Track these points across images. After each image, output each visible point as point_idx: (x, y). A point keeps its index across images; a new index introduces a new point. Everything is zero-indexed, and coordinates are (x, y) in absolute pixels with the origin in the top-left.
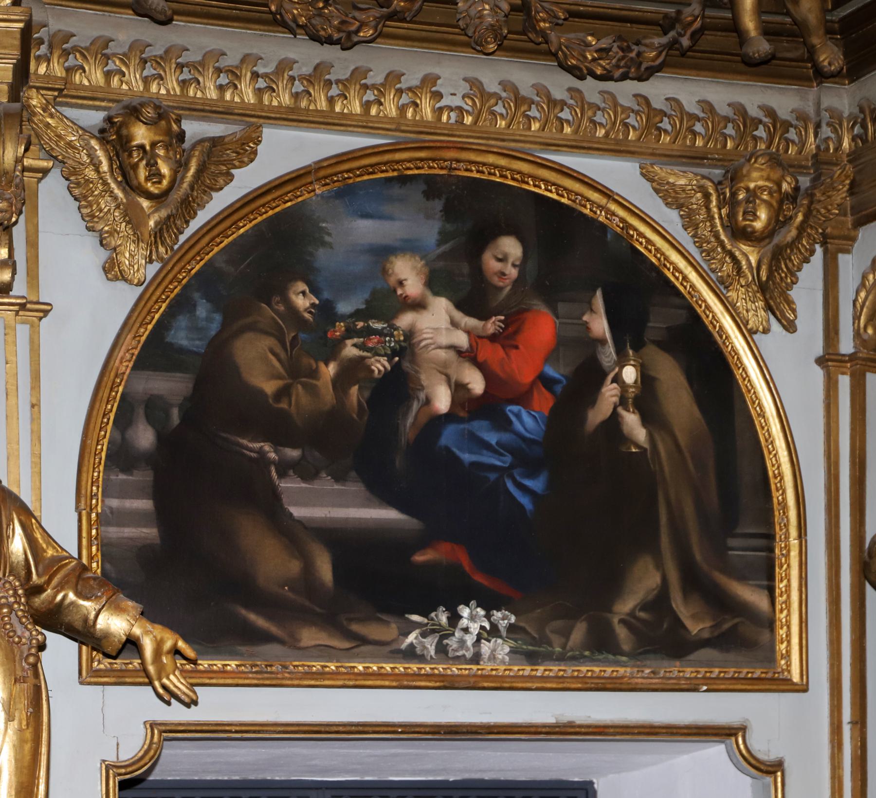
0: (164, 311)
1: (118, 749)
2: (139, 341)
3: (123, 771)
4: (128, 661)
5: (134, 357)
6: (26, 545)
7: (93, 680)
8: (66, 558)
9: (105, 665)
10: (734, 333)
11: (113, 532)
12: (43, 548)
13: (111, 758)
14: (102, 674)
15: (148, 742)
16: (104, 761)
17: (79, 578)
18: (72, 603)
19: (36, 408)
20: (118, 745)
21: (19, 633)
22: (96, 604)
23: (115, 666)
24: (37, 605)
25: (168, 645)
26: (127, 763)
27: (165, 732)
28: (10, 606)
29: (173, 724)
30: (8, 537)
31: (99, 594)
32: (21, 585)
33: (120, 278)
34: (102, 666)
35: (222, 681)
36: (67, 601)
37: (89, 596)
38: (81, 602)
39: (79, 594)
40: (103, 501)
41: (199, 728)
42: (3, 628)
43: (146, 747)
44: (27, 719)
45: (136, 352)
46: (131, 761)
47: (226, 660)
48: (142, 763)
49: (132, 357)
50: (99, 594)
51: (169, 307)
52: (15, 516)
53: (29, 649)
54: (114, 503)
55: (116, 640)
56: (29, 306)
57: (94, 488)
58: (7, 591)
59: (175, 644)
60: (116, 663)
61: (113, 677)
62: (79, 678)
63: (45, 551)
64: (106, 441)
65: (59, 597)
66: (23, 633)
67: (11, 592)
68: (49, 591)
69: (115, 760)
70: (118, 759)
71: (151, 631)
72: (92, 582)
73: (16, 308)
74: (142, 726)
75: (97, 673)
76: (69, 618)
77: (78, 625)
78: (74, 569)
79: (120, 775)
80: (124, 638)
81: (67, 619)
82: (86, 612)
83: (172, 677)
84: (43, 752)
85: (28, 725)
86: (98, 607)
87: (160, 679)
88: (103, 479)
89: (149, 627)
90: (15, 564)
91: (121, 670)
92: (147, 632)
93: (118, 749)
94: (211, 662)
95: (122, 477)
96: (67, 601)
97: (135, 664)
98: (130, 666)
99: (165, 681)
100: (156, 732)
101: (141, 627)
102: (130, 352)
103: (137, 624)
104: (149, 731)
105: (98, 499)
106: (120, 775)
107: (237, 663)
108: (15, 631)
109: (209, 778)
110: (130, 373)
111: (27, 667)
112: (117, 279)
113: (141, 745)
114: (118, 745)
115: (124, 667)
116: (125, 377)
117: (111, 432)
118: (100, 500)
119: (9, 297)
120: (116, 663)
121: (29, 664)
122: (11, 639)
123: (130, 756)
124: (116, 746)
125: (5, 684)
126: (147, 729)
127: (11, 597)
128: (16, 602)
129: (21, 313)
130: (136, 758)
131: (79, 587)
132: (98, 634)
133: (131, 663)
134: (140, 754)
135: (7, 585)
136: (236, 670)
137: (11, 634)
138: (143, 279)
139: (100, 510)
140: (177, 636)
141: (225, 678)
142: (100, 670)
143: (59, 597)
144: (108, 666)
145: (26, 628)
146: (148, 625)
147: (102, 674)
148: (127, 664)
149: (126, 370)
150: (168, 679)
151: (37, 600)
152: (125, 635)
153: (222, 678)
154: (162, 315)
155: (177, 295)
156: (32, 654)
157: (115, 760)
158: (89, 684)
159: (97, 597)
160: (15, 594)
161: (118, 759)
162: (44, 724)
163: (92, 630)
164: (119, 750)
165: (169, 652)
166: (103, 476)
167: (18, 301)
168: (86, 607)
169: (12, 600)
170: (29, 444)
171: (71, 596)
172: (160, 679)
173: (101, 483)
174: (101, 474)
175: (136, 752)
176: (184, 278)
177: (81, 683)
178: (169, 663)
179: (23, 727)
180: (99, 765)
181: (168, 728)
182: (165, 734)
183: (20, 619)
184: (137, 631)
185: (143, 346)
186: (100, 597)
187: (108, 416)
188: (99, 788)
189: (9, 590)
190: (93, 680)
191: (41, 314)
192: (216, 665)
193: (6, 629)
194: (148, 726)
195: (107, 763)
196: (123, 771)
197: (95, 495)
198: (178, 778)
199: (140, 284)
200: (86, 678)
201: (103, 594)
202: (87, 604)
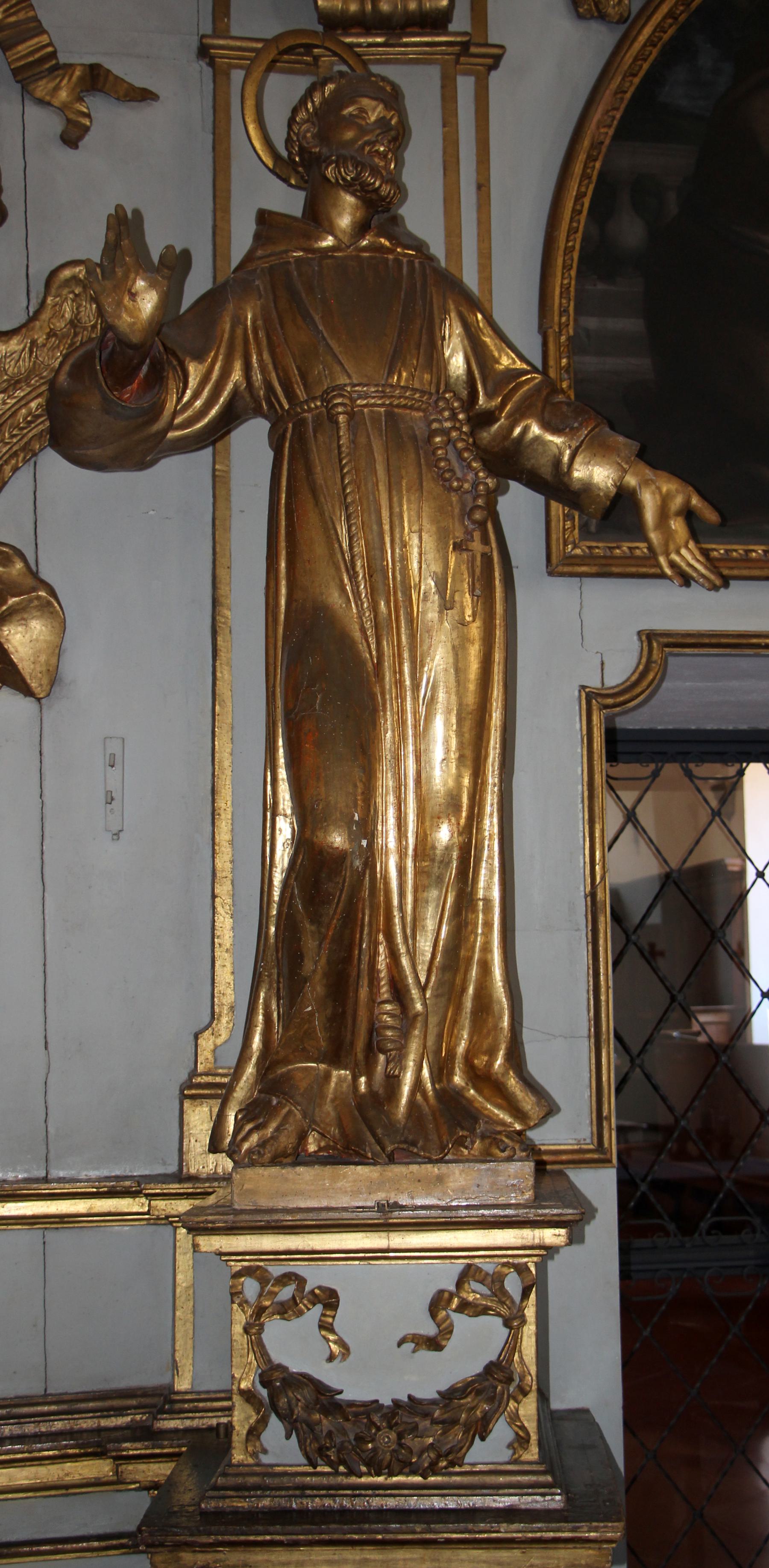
0: (656, 60)
1: (602, 670)
2: (622, 99)
3: (610, 701)
4: (615, 545)
5: (615, 122)
6: (469, 349)
7: (566, 569)
8: (526, 372)
9: (583, 550)
10: (491, 877)
11: (591, 363)
12: (493, 356)
13: (594, 682)
14: (578, 561)
15: (644, 660)
16: (583, 687)
17: (546, 401)
18: (537, 438)
19: (483, 189)
20: (602, 664)
21: (459, 474)
22: (571, 439)
23: (597, 551)
24: (485, 442)
25: (678, 501)
26: (616, 690)
27: (668, 645)
28: (445, 432)
29: (678, 634)
30: (444, 338)
31: (576, 425)
32: (462, 406)
33: (596, 14)
34: (578, 551)
35: (745, 572)
36: (530, 435)
37: (561, 427)
38: (549, 437)
39: (547, 426)
40: (575, 320)
41: (714, 641)
42: (436, 466)
43: (641, 667)
44: (473, 608)
45: (618, 115)
46: (622, 687)
47: (748, 544)
48: (639, 690)
49: (612, 121)
50: (576, 425)
51: (662, 53)
52: (452, 307)
53: (475, 499)
54: (592, 323)
55: (601, 494)
56: (474, 50)
57: (564, 301)
58: (441, 412)
59: (688, 501)
60: (598, 547)
61: (595, 565)
62: (547, 567)
63: (497, 362)
64: (579, 235)
65: (517, 431)
66: (465, 475)
67: (446, 414)
68: (503, 420)
69: (599, 685)
70: (603, 684)
71: (651, 480)
72: (565, 408)
73: (456, 49)
74: (635, 638)
75: (571, 560)
76: (533, 461)
77: (546, 471)
78: (538, 389)
79: (606, 707)
80: (613, 490)
81: (529, 465)
82: (556, 451)
83: (683, 551)
84: (497, 660)
85: (474, 615)
86: (574, 444)
87: (667, 554)
88: (576, 290)
89: (649, 473)
90: (452, 380)
91: (605, 557)
92: (646, 482)
93: (602, 670)
94: (729, 547)
95: (601, 286)
96: (530, 435)
97: (625, 548)
98: (618, 551)
99: (674, 557)
100: (655, 645)
101: (635, 474)
102: (610, 114)
103: (631, 470)
104: (645, 644)
105: (569, 316)
106: (606, 707)
107: (763, 547)
108: (452, 471)
109: (709, 727)
110: (610, 145)
111: (471, 527)
112: (592, 17)
113: (634, 665)
114: (602, 664)
115: (608, 553)
116: (604, 149)
117: (586, 223)
118: (571, 318)
119: (446, 33)
120: (598, 547)
121: (474, 522)
122: (447, 484)
123: (619, 681)
124: (600, 666)
125: (438, 551)
126: (642, 642)
127: (446, 420)
128: (454, 428)
129: (462, 59)
130: (629, 683)
131: (546, 415)
132: (576, 486)
133: (618, 547)
134: (634, 678)
135: (441, 404)
136: (764, 558)
137: (447, 475)
138: (626, 15)
139: (571, 332)
140: (690, 488)
141: (749, 568)
142: (576, 556)
143: (517, 431)
144: (587, 551)
145: (469, 466)
146: (647, 471)
147: (578, 561)
148: (614, 548)
149: (605, 138)
150: (678, 553)
151: (485, 434)
152: (615, 485)
153: (745, 568)
154: (652, 66)
155: (672, 39)
156: (479, 507)
157: (599, 685)
158: (562, 575)
159: (572, 429)
160: (454, 417)
161: (603, 684)
162: (498, 617)
163: (566, 479)
164: (605, 671)
165: (678, 514)
166: (576, 284)
167: (459, 39)
168: (557, 444)
169: (448, 425)
170: (476, 239)
171: (535, 430)
172: (667, 554)
173: (572, 294)
174: (573, 282)
175: (628, 674)
176: (682, 12)
177: (551, 574)
178: (679, 529)
179: (468, 619)
180: (576, 693)
181: (671, 640)
182: (666, 649)
183: (459, 454)
184: (631, 480)
185: (628, 106)
186: (578, 429)
187: (581, 201)
188: (578, 726)
189: (444, 410)
190: (566, 569)
191: (490, 61)
192: (736, 551)
193: (439, 468)
194: (644, 638)
195: (587, 690)
196: (610, 701)
197: (564, 311)
198: (671, 727)
199: (622, 20)
200: (557, 566)
201: (581, 424)
202: (558, 440)
